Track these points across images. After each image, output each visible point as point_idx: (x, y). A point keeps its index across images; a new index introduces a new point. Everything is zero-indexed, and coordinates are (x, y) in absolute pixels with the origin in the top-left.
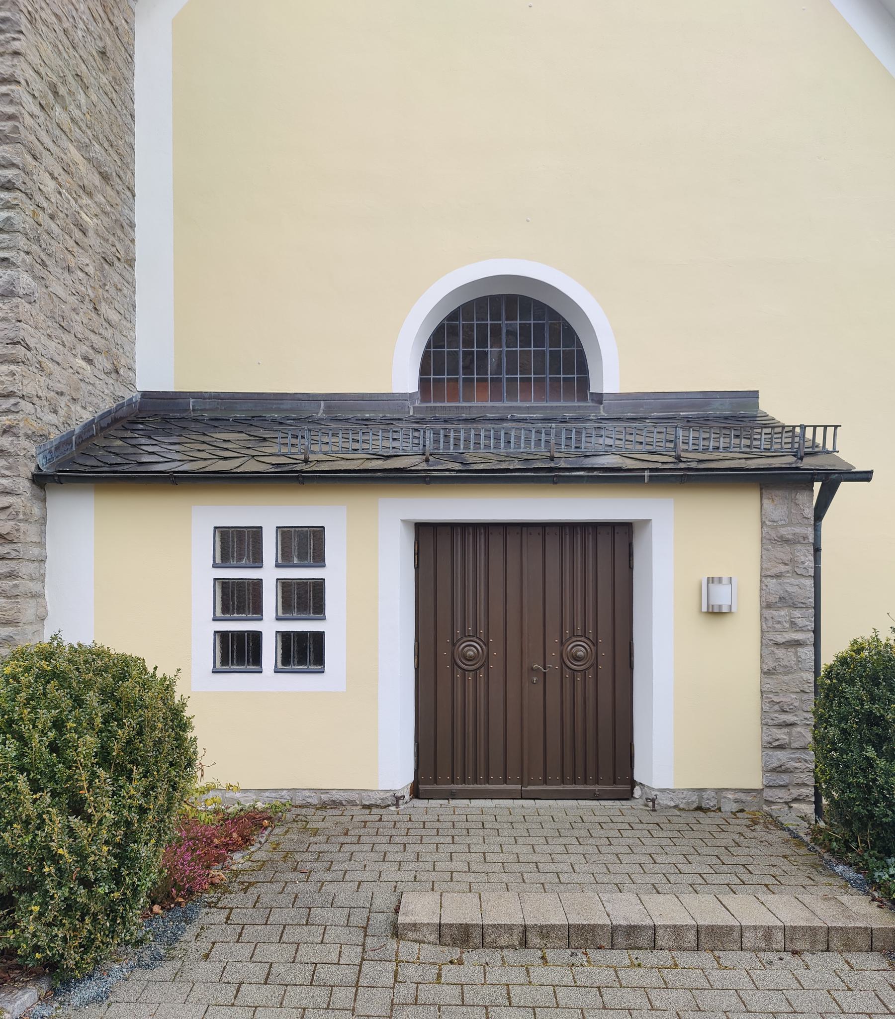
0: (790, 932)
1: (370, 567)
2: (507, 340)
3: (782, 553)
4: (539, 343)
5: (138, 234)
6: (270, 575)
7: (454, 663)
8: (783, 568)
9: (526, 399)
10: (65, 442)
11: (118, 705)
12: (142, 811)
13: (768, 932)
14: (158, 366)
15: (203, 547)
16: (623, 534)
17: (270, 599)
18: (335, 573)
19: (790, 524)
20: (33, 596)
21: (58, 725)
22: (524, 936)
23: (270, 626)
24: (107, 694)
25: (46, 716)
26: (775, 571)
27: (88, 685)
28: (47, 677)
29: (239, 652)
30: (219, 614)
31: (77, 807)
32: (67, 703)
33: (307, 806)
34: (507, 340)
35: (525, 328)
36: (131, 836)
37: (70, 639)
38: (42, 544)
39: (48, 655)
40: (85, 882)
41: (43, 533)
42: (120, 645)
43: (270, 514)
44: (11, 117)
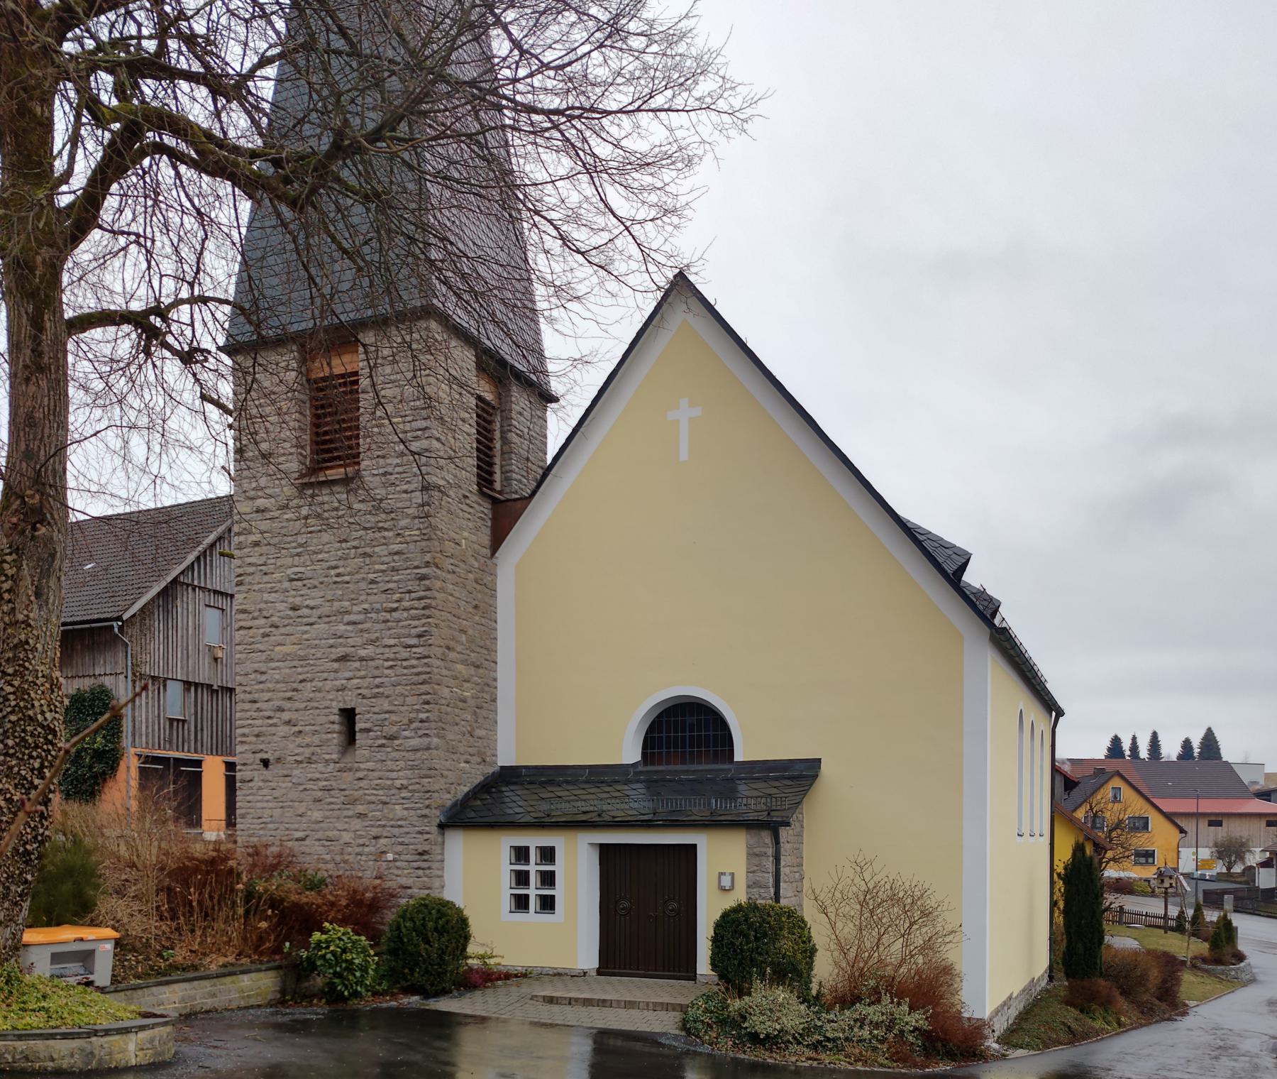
0: (655, 1004)
1: (577, 865)
2: (687, 731)
3: (755, 860)
4: (676, 747)
5: (499, 684)
6: (533, 868)
10: (455, 805)
11: (441, 914)
13: (648, 1004)
14: (507, 755)
15: (505, 855)
16: (693, 848)
18: (559, 867)
23: (533, 891)
24: (439, 911)
29: (521, 903)
31: (428, 942)
34: (687, 731)
35: (699, 721)
38: (442, 854)
43: (534, 841)
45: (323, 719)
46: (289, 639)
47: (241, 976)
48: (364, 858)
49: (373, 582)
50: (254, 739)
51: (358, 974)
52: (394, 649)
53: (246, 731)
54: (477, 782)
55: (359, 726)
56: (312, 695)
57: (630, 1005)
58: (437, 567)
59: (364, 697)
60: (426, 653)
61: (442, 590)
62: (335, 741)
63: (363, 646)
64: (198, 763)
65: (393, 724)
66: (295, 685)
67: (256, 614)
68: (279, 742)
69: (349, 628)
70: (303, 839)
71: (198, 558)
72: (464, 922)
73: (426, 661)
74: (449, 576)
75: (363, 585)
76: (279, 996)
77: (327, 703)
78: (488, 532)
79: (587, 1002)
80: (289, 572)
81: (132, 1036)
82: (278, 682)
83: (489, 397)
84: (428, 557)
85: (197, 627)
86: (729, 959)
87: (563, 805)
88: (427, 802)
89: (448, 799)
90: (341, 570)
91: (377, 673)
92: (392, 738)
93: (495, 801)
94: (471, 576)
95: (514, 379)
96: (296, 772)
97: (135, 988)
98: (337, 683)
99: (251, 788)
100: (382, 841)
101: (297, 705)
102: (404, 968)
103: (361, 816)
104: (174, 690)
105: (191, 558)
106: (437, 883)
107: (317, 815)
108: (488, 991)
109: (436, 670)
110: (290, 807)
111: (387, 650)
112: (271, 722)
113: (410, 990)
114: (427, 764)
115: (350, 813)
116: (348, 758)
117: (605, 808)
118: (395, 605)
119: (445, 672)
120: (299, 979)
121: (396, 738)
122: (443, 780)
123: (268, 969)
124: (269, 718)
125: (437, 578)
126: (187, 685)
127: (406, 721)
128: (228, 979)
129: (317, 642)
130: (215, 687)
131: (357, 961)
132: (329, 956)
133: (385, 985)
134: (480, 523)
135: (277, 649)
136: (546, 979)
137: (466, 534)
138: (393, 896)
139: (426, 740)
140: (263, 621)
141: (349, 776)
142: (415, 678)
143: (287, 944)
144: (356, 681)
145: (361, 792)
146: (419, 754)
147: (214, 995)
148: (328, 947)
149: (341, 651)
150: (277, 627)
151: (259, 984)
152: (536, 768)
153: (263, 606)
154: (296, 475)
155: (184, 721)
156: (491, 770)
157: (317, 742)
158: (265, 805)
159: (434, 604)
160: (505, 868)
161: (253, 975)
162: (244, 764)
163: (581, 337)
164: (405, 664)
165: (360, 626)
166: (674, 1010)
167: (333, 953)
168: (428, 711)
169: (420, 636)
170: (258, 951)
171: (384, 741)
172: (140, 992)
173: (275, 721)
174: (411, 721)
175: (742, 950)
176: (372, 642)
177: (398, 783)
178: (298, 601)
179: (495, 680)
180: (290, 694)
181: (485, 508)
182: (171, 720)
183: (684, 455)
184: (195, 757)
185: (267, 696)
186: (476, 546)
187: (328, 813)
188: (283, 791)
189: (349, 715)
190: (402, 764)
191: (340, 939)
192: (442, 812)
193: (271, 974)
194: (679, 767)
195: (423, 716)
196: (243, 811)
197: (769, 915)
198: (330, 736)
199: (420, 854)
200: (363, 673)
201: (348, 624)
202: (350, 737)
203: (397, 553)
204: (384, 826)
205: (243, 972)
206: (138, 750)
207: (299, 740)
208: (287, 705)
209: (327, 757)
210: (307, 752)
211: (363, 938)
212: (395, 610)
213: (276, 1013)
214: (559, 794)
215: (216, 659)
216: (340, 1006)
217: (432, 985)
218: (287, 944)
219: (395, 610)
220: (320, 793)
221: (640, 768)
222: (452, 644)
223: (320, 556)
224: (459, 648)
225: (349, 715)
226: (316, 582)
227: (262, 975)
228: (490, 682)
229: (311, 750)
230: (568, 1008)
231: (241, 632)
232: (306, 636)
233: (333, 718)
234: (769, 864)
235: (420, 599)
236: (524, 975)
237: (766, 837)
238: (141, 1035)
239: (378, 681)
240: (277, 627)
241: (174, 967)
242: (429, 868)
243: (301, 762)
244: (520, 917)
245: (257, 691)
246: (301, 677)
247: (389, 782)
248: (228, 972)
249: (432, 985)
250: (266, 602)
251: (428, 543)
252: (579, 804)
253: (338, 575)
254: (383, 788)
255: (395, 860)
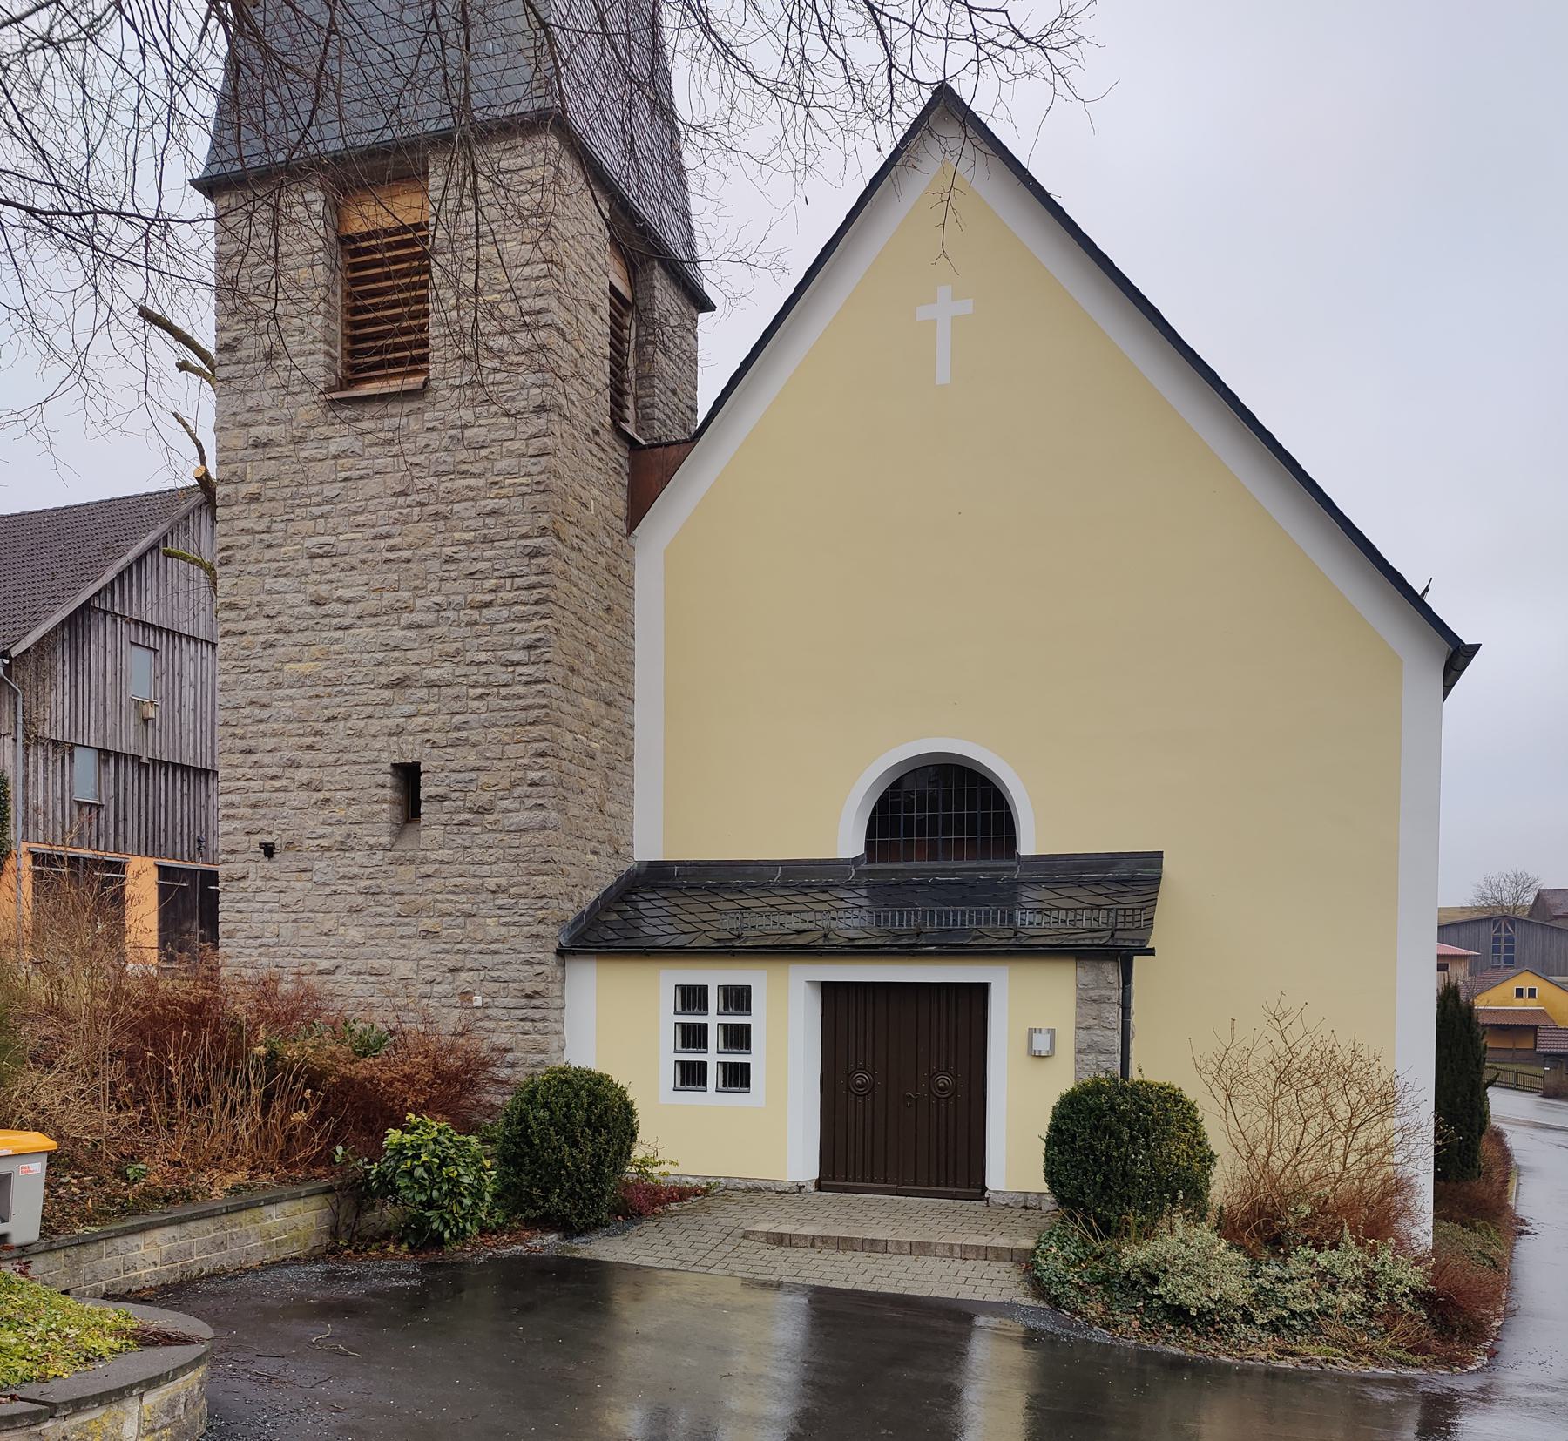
0: (964, 1248)
1: (787, 1017)
2: (942, 812)
3: (1092, 1010)
4: (933, 832)
5: (637, 733)
7: (848, 1088)
8: (1092, 1022)
9: (959, 858)
10: (579, 920)
11: (596, 1098)
12: (606, 1152)
17: (713, 1037)
18: (757, 1019)
19: (1098, 987)
20: (557, 1033)
21: (568, 1105)
22: (812, 1242)
23: (713, 1057)
25: (562, 1100)
26: (1086, 1024)
27: (582, 1087)
28: (562, 1082)
29: (692, 1076)
30: (679, 1048)
31: (575, 1144)
32: (571, 1095)
33: (738, 1189)
34: (942, 812)
36: (601, 1163)
37: (574, 1064)
38: (562, 997)
39: (563, 1071)
40: (579, 1181)
41: (563, 988)
42: (598, 1068)
43: (714, 976)
44: (545, 707)
45: (366, 781)
46: (307, 652)
47: (265, 1209)
48: (433, 1002)
49: (450, 560)
50: (248, 811)
51: (467, 1202)
52: (486, 669)
53: (234, 798)
54: (607, 884)
55: (424, 793)
56: (347, 742)
57: (920, 1249)
58: (559, 538)
59: (435, 745)
60: (541, 675)
61: (564, 575)
62: (386, 816)
63: (433, 663)
64: (119, 867)
65: (486, 787)
66: (318, 726)
67: (253, 611)
68: (290, 815)
69: (411, 634)
70: (332, 972)
71: (121, 575)
72: (628, 1110)
73: (540, 687)
74: (573, 555)
75: (434, 565)
76: (327, 1240)
77: (372, 755)
78: (623, 493)
79: (844, 1244)
80: (309, 543)
81: (132, 1405)
82: (289, 721)
83: (623, 288)
84: (544, 520)
85: (118, 673)
86: (1085, 1172)
87: (758, 921)
88: (540, 914)
89: (570, 910)
90: (396, 541)
91: (456, 706)
92: (483, 811)
93: (633, 914)
94: (602, 560)
95: (653, 265)
96: (318, 865)
97: (84, 1243)
98: (390, 722)
99: (244, 890)
100: (463, 975)
101: (321, 757)
102: (531, 1186)
103: (428, 935)
104: (85, 762)
105: (110, 574)
106: (554, 1043)
107: (354, 933)
108: (665, 1222)
109: (556, 704)
110: (308, 920)
111: (474, 669)
112: (277, 784)
113: (545, 1223)
114: (541, 853)
115: (411, 931)
116: (407, 845)
117: (833, 925)
118: (488, 598)
119: (567, 708)
120: (359, 1210)
121: (488, 811)
122: (563, 880)
123: (310, 1195)
124: (274, 777)
125: (557, 555)
126: (104, 754)
127: (505, 784)
128: (245, 1216)
129: (355, 656)
130: (144, 760)
131: (465, 1180)
132: (419, 1172)
133: (499, 1216)
134: (614, 478)
135: (287, 667)
136: (737, 1196)
137: (595, 492)
138: (485, 1064)
139: (539, 815)
140: (264, 623)
141: (408, 872)
142: (523, 715)
143: (339, 1149)
144: (420, 720)
145: (429, 898)
146: (526, 838)
147: (221, 1246)
148: (417, 1156)
149: (396, 671)
150: (288, 632)
151: (291, 1221)
152: (696, 863)
153: (264, 598)
154: (322, 386)
155: (99, 807)
156: (625, 867)
157: (355, 817)
158: (267, 916)
159: (553, 596)
160: (667, 1019)
161: (286, 1206)
162: (233, 852)
163: (759, 200)
164: (504, 691)
165: (429, 631)
166: (998, 1258)
167: (427, 1167)
168: (543, 768)
169: (530, 647)
170: (285, 1163)
171: (467, 816)
172: (93, 1249)
173: (284, 782)
174: (513, 785)
175: (1109, 1158)
176: (449, 657)
177: (491, 883)
178: (323, 590)
179: (632, 727)
180: (309, 740)
181: (620, 455)
182: (80, 805)
183: (943, 375)
184: (113, 857)
185: (271, 742)
186: (609, 514)
187: (374, 931)
188: (298, 895)
189: (408, 775)
190: (497, 852)
191: (435, 1141)
192: (562, 931)
193: (315, 1202)
194: (927, 864)
195: (535, 775)
196: (231, 926)
197: (1149, 1101)
198: (376, 807)
199: (528, 997)
200: (432, 707)
201: (408, 627)
202: (410, 807)
203: (491, 514)
204: (467, 952)
205: (269, 1202)
206: (35, 847)
207: (324, 814)
208: (306, 757)
209: (372, 841)
210: (339, 833)
211: (473, 1139)
212: (488, 605)
213: (333, 1277)
214: (746, 904)
215: (146, 721)
216: (432, 1256)
217: (581, 1215)
218: (339, 1149)
219: (488, 605)
220: (360, 899)
221: (864, 866)
222: (577, 664)
223: (361, 519)
224: (587, 672)
225: (408, 775)
226: (355, 561)
227: (300, 1204)
228: (626, 731)
229: (345, 829)
230: (813, 1254)
231: (227, 640)
232: (336, 647)
233: (381, 778)
234: (1115, 1015)
235: (529, 587)
236: (705, 1192)
237: (1111, 972)
238: (153, 1398)
239: (457, 719)
240: (288, 632)
241: (149, 1197)
242: (543, 1019)
243: (328, 849)
244: (691, 1097)
245: (254, 735)
246: (327, 713)
247: (477, 882)
248: (244, 1202)
249: (581, 1215)
250: (270, 592)
251: (544, 497)
252: (812, 916)
253: (391, 549)
254: (466, 891)
255: (485, 1007)
